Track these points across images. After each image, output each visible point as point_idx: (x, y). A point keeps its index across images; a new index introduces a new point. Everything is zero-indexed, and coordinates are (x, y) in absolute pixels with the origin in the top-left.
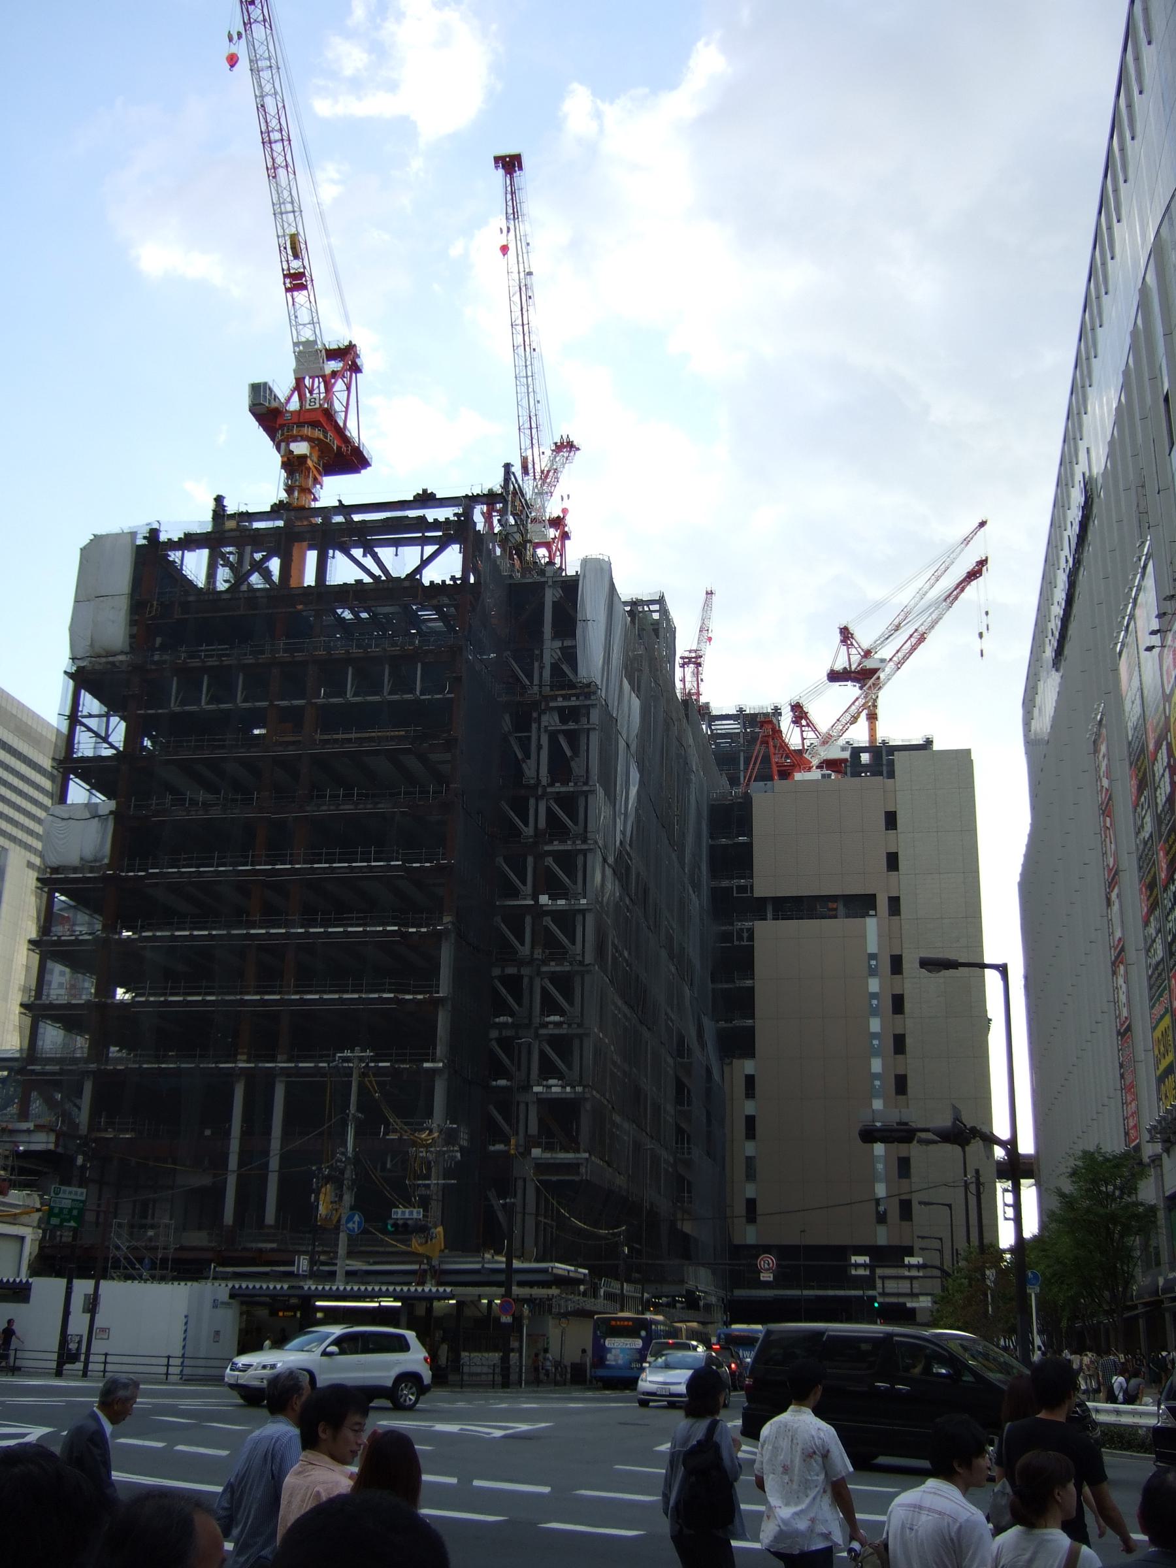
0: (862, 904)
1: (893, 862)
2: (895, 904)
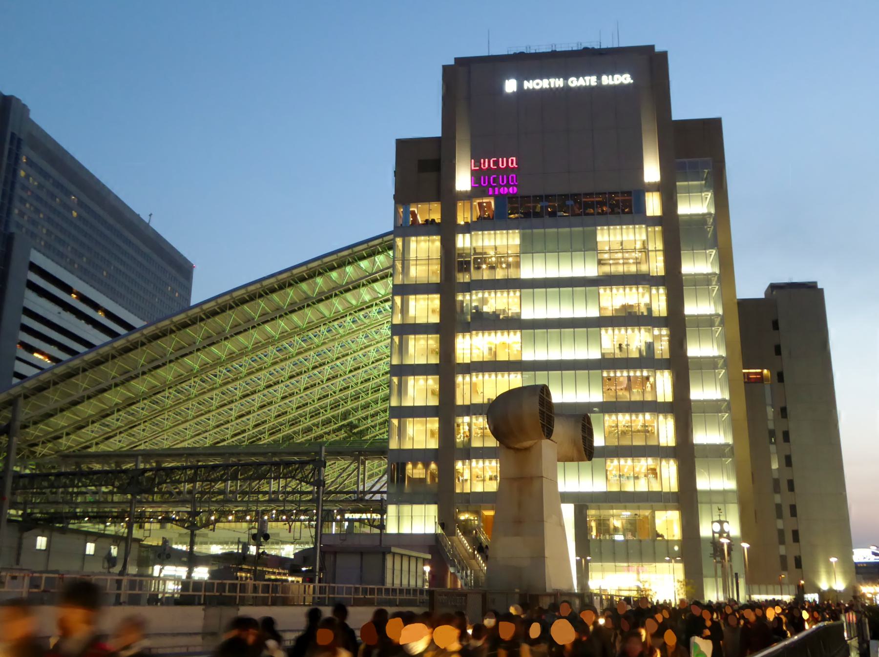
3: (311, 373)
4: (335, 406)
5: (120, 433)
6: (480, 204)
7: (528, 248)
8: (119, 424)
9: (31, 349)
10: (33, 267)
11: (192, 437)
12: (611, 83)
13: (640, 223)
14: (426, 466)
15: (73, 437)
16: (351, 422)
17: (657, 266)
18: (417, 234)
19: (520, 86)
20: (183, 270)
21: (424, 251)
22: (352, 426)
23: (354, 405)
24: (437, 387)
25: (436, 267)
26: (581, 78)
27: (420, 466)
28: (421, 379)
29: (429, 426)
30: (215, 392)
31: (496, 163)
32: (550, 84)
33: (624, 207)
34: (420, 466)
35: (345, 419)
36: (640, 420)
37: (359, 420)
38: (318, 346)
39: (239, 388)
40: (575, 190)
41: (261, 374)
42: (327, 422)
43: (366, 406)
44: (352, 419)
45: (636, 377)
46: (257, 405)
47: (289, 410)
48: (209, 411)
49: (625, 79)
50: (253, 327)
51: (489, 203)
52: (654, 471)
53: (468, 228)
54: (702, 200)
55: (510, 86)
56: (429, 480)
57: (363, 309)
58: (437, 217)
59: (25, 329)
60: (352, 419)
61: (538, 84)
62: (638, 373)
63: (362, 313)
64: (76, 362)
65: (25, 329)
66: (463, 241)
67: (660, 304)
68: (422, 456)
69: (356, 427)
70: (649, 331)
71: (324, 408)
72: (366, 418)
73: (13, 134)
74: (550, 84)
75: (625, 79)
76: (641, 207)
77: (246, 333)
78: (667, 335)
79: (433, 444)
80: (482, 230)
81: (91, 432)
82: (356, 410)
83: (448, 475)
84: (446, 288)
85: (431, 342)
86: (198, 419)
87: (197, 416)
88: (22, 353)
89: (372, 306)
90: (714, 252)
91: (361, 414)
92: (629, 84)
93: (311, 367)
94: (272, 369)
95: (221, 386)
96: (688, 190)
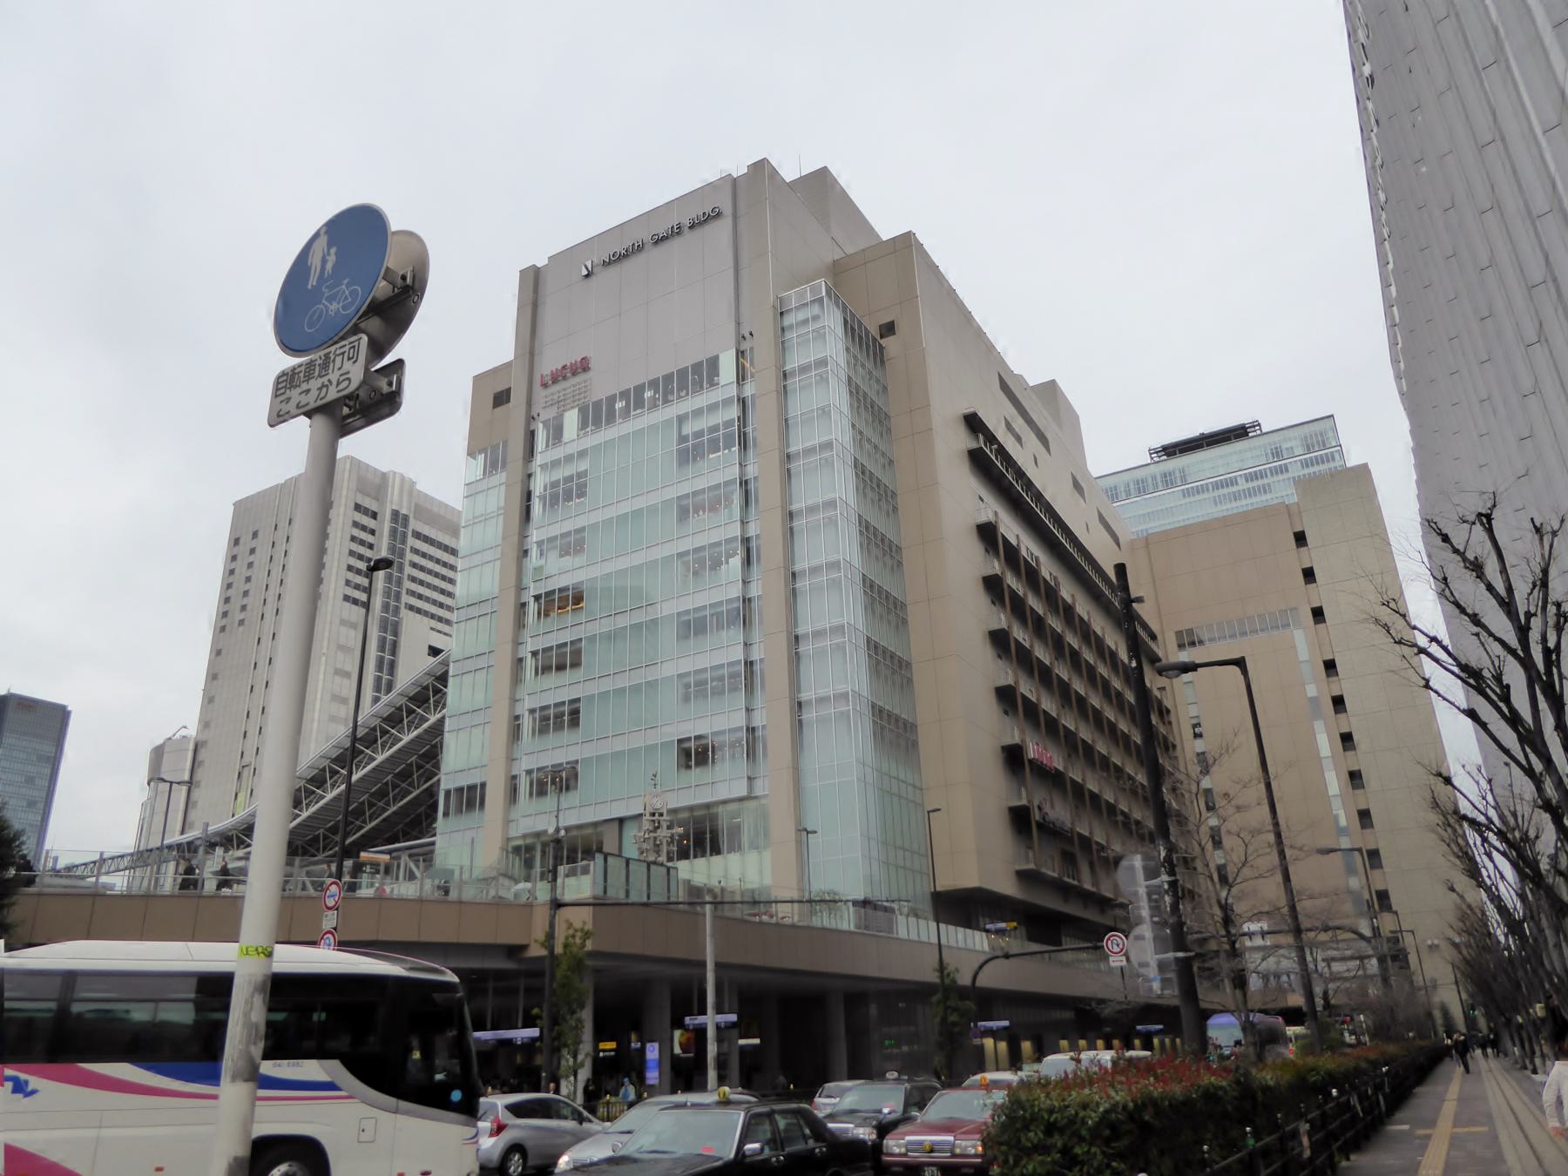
0: (1282, 621)
1: (1309, 575)
2: (1318, 614)
73: (395, 514)
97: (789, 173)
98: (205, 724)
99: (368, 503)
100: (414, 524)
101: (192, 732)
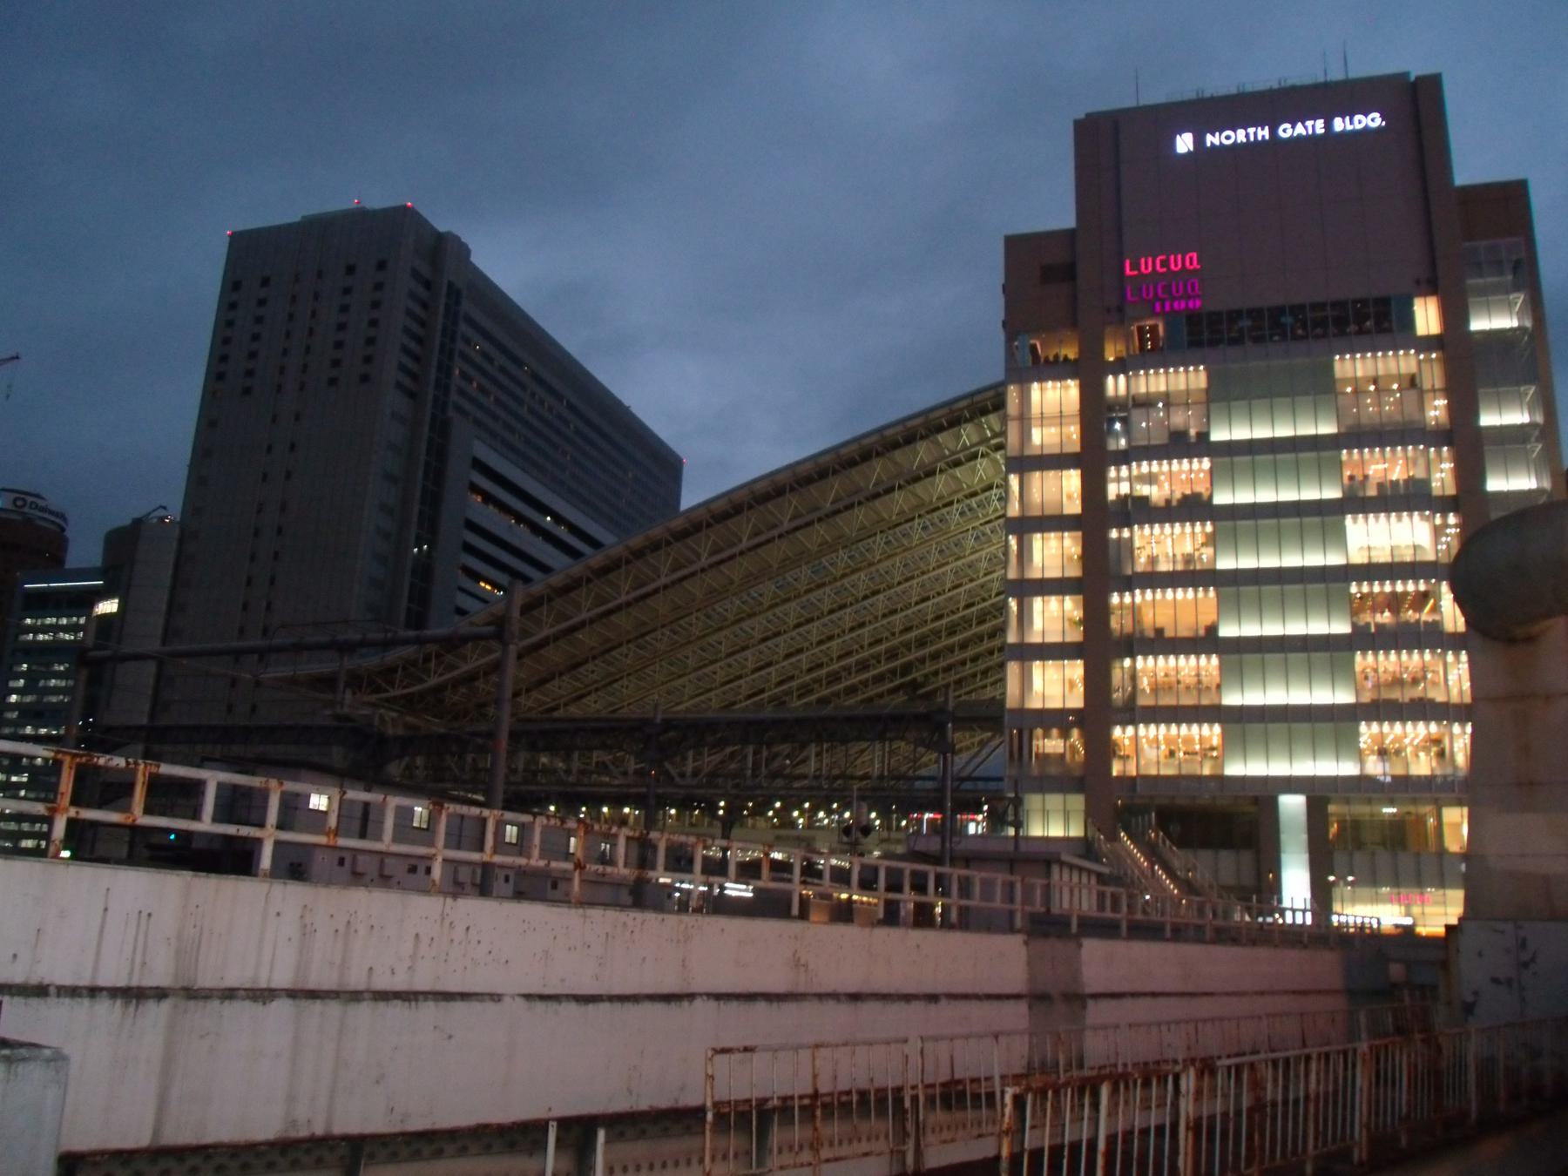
3: (826, 620)
4: (892, 654)
5: (597, 690)
6: (1141, 330)
7: (1220, 396)
8: (595, 676)
9: (477, 577)
10: (480, 466)
11: (692, 698)
12: (1349, 127)
13: (1407, 348)
14: (1065, 735)
15: (534, 694)
16: (914, 680)
17: (1437, 410)
18: (1041, 379)
19: (1199, 141)
20: (667, 466)
21: (1053, 405)
22: (914, 685)
23: (920, 653)
24: (1078, 614)
25: (1074, 431)
26: (1299, 125)
27: (1055, 732)
28: (1053, 602)
29: (1068, 672)
30: (725, 632)
31: (1165, 263)
32: (1247, 136)
33: (1382, 322)
34: (1055, 732)
35: (903, 675)
36: (1413, 660)
37: (926, 676)
38: (835, 580)
39: (756, 627)
40: (1297, 300)
41: (754, 621)
42: (879, 679)
43: (935, 657)
44: (916, 675)
45: (1405, 594)
46: (782, 651)
47: (797, 673)
48: (716, 661)
49: (1374, 120)
50: (820, 520)
51: (1154, 329)
52: (1437, 741)
53: (1121, 367)
54: (1510, 306)
55: (1184, 143)
56: (1068, 756)
57: (938, 508)
58: (1071, 353)
59: (469, 549)
60: (916, 675)
61: (1228, 138)
62: (1411, 587)
63: (936, 514)
64: (577, 569)
65: (469, 549)
66: (1116, 386)
67: (1443, 477)
68: (1055, 719)
69: (922, 686)
70: (1427, 519)
71: (847, 669)
72: (936, 673)
73: (450, 285)
74: (1247, 136)
75: (1374, 120)
76: (1408, 321)
77: (809, 529)
78: (1456, 526)
79: (1076, 701)
80: (1146, 368)
81: (561, 687)
82: (922, 660)
83: (1101, 749)
84: (1092, 460)
85: (1068, 542)
86: (700, 673)
87: (700, 668)
88: (467, 583)
89: (951, 503)
90: (1532, 390)
91: (929, 668)
92: (1379, 128)
93: (826, 610)
94: (769, 614)
95: (733, 623)
96: (1484, 292)
97: (1053, 208)
98: (193, 504)
99: (425, 270)
100: (466, 306)
101: (174, 513)
